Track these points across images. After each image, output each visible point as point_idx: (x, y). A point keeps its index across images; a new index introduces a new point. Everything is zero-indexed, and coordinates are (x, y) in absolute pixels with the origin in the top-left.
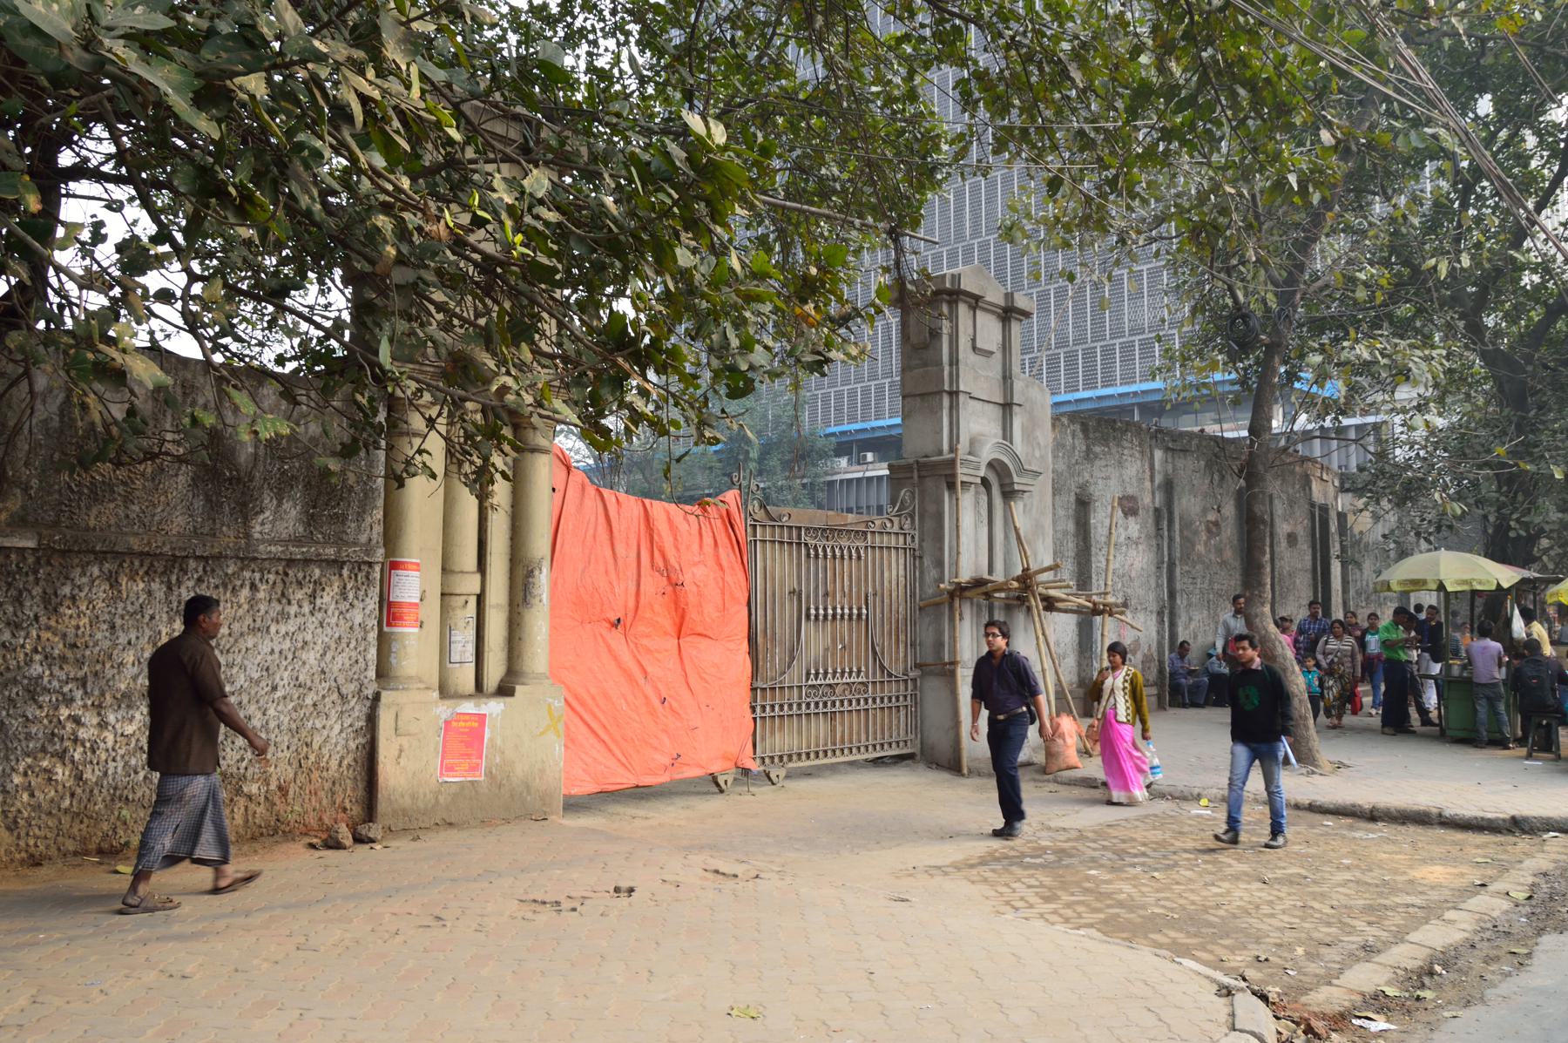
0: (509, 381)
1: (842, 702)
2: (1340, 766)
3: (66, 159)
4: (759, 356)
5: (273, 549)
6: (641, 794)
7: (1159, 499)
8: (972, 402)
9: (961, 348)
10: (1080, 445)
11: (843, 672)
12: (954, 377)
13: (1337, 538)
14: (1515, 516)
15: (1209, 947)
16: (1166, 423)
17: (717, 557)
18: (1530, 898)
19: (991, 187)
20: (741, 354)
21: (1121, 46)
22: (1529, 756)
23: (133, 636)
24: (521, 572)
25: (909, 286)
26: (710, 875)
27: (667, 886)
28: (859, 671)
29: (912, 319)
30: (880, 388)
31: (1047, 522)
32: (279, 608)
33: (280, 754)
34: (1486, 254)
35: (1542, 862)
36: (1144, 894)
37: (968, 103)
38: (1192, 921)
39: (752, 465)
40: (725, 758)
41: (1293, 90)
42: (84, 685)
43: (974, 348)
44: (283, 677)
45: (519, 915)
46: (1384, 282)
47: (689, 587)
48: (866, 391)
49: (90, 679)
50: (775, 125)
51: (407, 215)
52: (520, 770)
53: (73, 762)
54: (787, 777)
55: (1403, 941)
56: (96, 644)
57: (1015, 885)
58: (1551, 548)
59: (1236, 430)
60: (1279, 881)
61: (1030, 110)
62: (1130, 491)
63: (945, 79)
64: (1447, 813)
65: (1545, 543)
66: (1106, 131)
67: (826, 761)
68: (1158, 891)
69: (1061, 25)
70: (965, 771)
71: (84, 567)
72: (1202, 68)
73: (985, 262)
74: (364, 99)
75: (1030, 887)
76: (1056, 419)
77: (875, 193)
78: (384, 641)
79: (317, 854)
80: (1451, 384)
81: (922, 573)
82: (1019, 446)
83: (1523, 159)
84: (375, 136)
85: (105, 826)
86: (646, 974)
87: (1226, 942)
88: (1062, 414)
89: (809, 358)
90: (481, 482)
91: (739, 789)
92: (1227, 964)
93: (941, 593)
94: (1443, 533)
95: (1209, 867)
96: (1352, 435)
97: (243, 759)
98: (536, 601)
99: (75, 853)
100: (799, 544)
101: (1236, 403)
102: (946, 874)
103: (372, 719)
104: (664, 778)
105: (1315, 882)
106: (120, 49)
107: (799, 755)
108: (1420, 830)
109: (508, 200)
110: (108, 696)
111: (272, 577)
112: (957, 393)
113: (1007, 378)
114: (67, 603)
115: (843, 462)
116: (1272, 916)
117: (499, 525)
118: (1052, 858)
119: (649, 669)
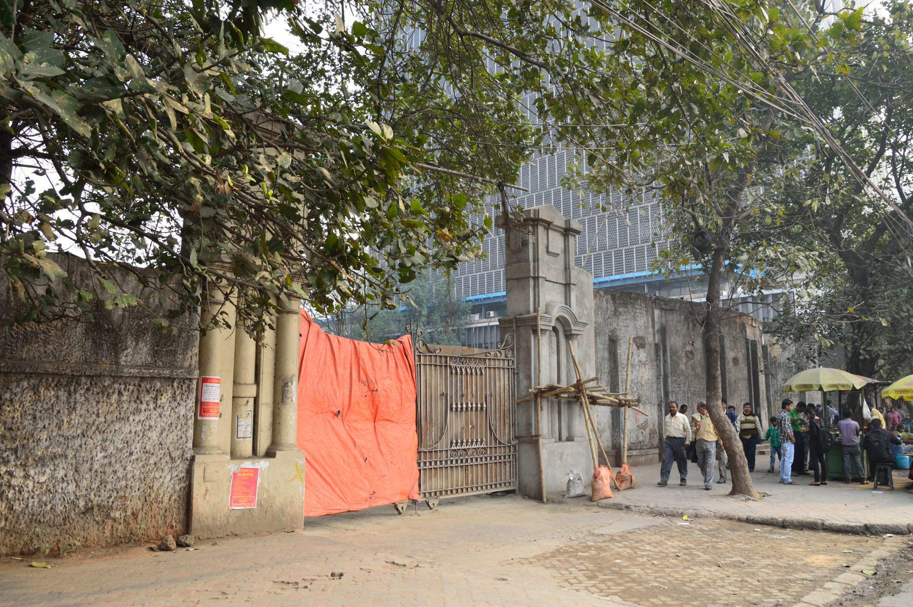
1: (472, 459)
2: (765, 495)
3: (15, 145)
4: (418, 258)
5: (132, 371)
6: (351, 516)
7: (658, 339)
10: (611, 307)
11: (472, 442)
12: (536, 269)
13: (762, 359)
14: (862, 347)
16: (663, 294)
17: (398, 374)
18: (875, 574)
19: (551, 161)
21: (629, 79)
22: (875, 488)
23: (47, 423)
24: (280, 384)
25: (510, 216)
26: (389, 565)
27: (363, 572)
29: (512, 235)
32: (135, 406)
33: (133, 494)
34: (840, 197)
35: (882, 552)
36: (647, 574)
37: (542, 112)
39: (423, 319)
40: (402, 493)
41: (725, 107)
42: (16, 453)
43: (548, 252)
44: (137, 447)
45: (273, 591)
46: (781, 213)
47: (381, 393)
48: (489, 276)
49: (20, 449)
50: (434, 124)
51: (208, 177)
52: (278, 502)
53: (7, 499)
54: (439, 504)
55: (799, 601)
56: (24, 428)
57: (571, 570)
58: (884, 365)
59: (700, 298)
60: (727, 565)
61: (578, 116)
62: (641, 334)
63: (525, 100)
64: (827, 523)
65: (881, 362)
67: (462, 495)
68: (656, 572)
69: (594, 69)
70: (545, 500)
71: (18, 382)
72: (673, 94)
73: (557, 203)
74: (179, 114)
75: (580, 570)
76: (596, 293)
78: (198, 426)
79: (154, 554)
80: (824, 270)
81: (518, 383)
82: (574, 308)
83: (860, 143)
84: (188, 134)
85: (26, 538)
88: (600, 289)
89: (445, 259)
90: (257, 331)
91: (410, 512)
93: (530, 394)
94: (824, 358)
95: (687, 557)
96: (770, 300)
97: (111, 497)
98: (289, 401)
99: (7, 555)
100: (446, 366)
102: (531, 563)
103: (190, 472)
105: (749, 566)
106: (29, 87)
107: (446, 491)
108: (811, 533)
109: (268, 170)
110: (30, 459)
111: (131, 388)
112: (538, 278)
113: (567, 269)
114: (7, 403)
115: (477, 317)
116: (723, 587)
117: (268, 356)
118: (594, 552)
119: (357, 441)
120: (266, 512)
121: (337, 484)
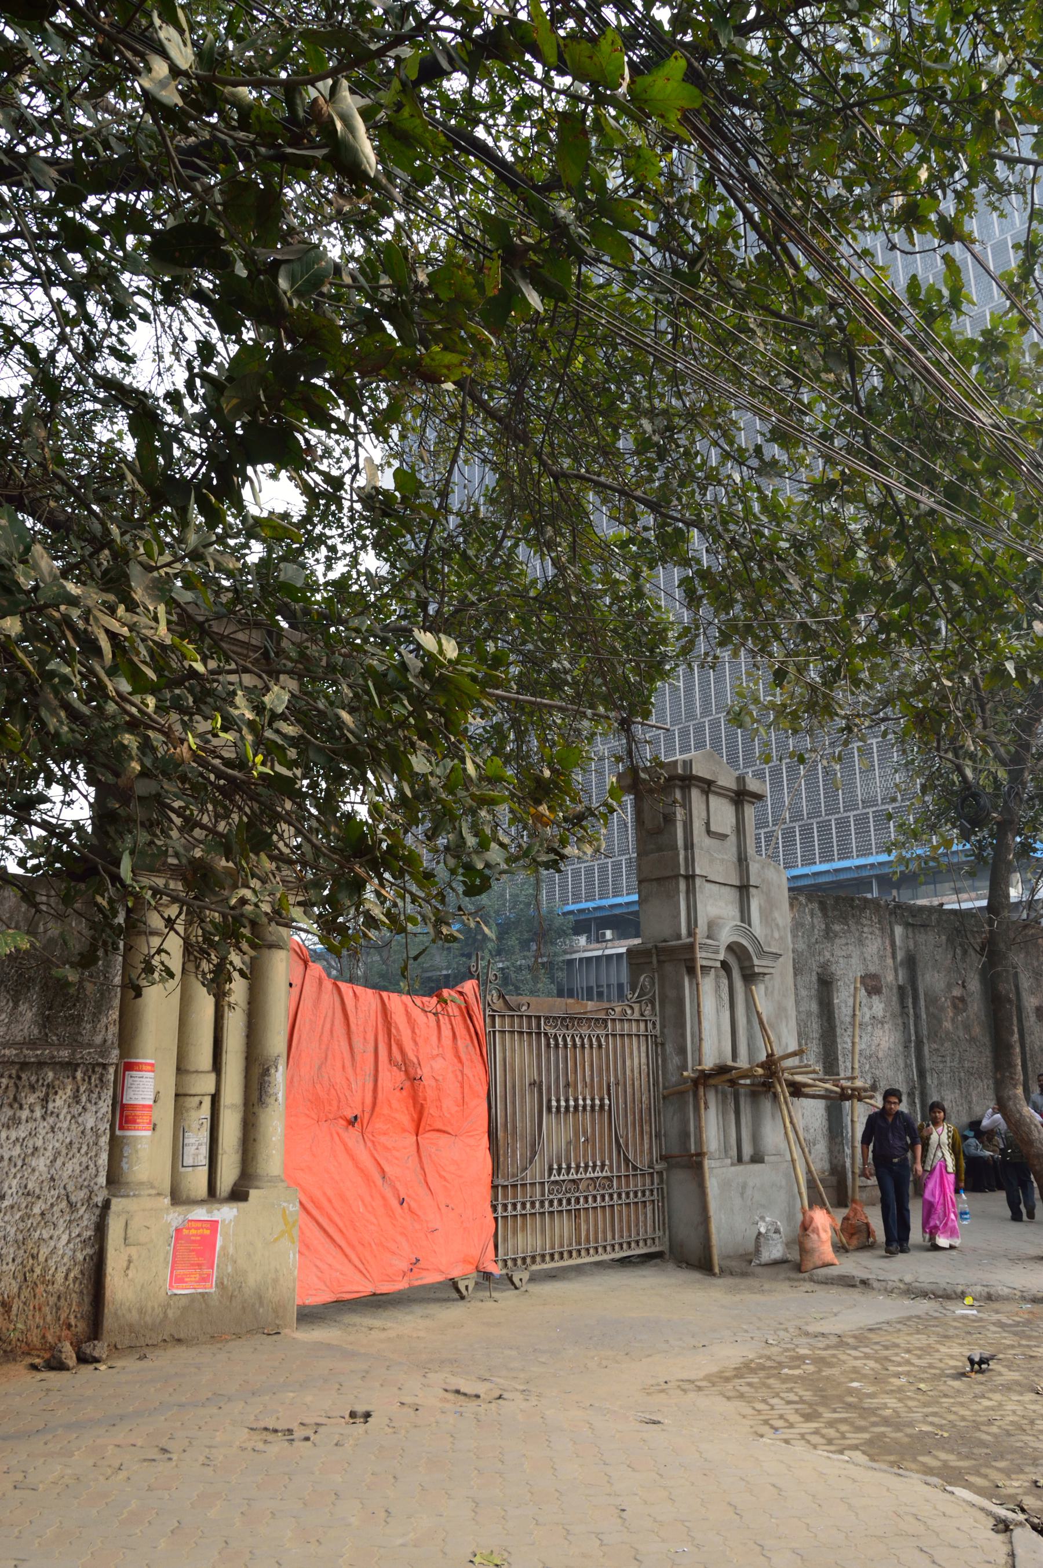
0: (247, 893)
1: (586, 1198)
4: (495, 854)
5: (7, 1052)
6: (377, 1302)
8: (708, 885)
9: (695, 832)
10: (819, 924)
12: (690, 861)
15: (983, 1470)
20: (477, 852)
24: (256, 1071)
25: (643, 775)
26: (451, 1396)
27: (405, 1409)
28: (603, 1165)
30: (617, 866)
31: (790, 1004)
32: (10, 1113)
36: (910, 1410)
37: (692, 600)
38: (963, 1439)
40: (465, 1261)
43: (709, 832)
45: (249, 1445)
47: (427, 1081)
48: (603, 869)
50: (508, 620)
51: (151, 733)
52: (253, 1280)
57: (775, 1401)
62: (872, 969)
66: (827, 623)
68: (925, 1405)
70: (717, 1270)
74: (112, 636)
75: (789, 1402)
77: (605, 683)
78: (116, 1146)
79: (40, 1376)
81: (664, 1061)
82: (758, 928)
86: (384, 1515)
87: (1001, 1464)
89: (543, 858)
92: (1003, 1491)
93: (685, 1080)
98: (271, 1100)
100: (538, 1034)
101: (972, 875)
102: (700, 1389)
103: (101, 1229)
104: (402, 1285)
109: (249, 715)
113: (742, 860)
115: (582, 940)
118: (811, 1368)
119: (387, 1168)
120: (231, 1298)
121: (353, 1247)
